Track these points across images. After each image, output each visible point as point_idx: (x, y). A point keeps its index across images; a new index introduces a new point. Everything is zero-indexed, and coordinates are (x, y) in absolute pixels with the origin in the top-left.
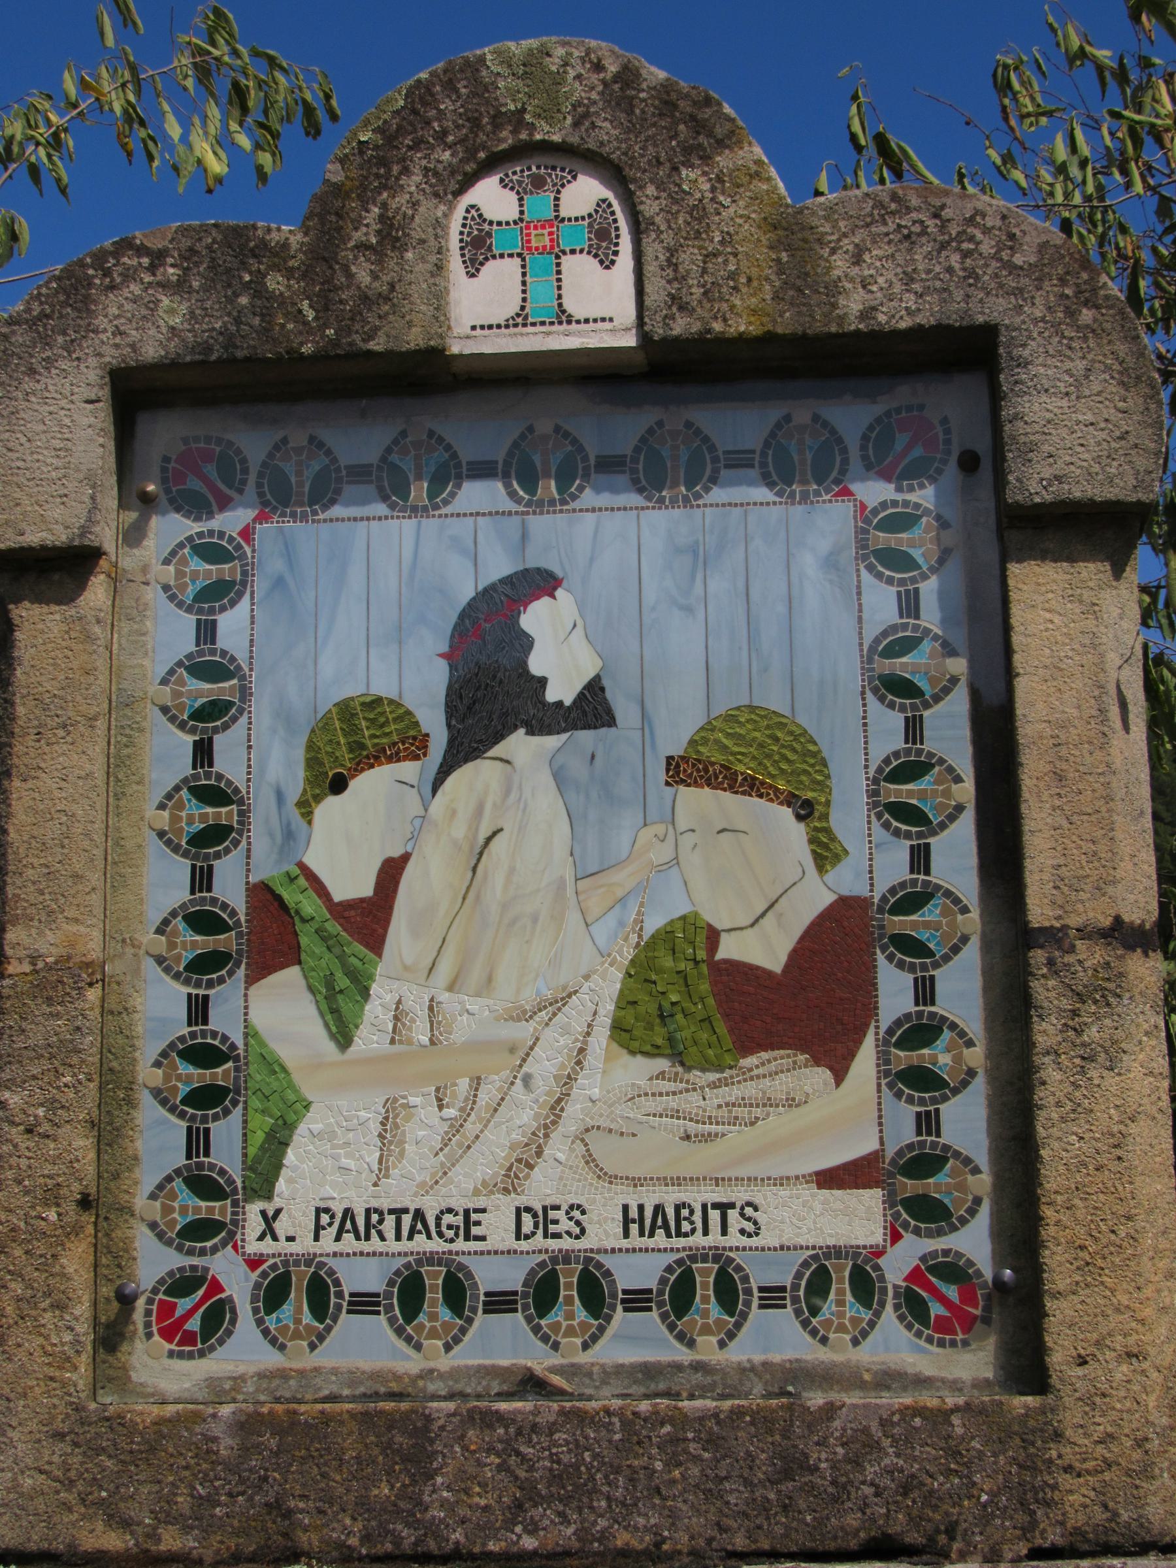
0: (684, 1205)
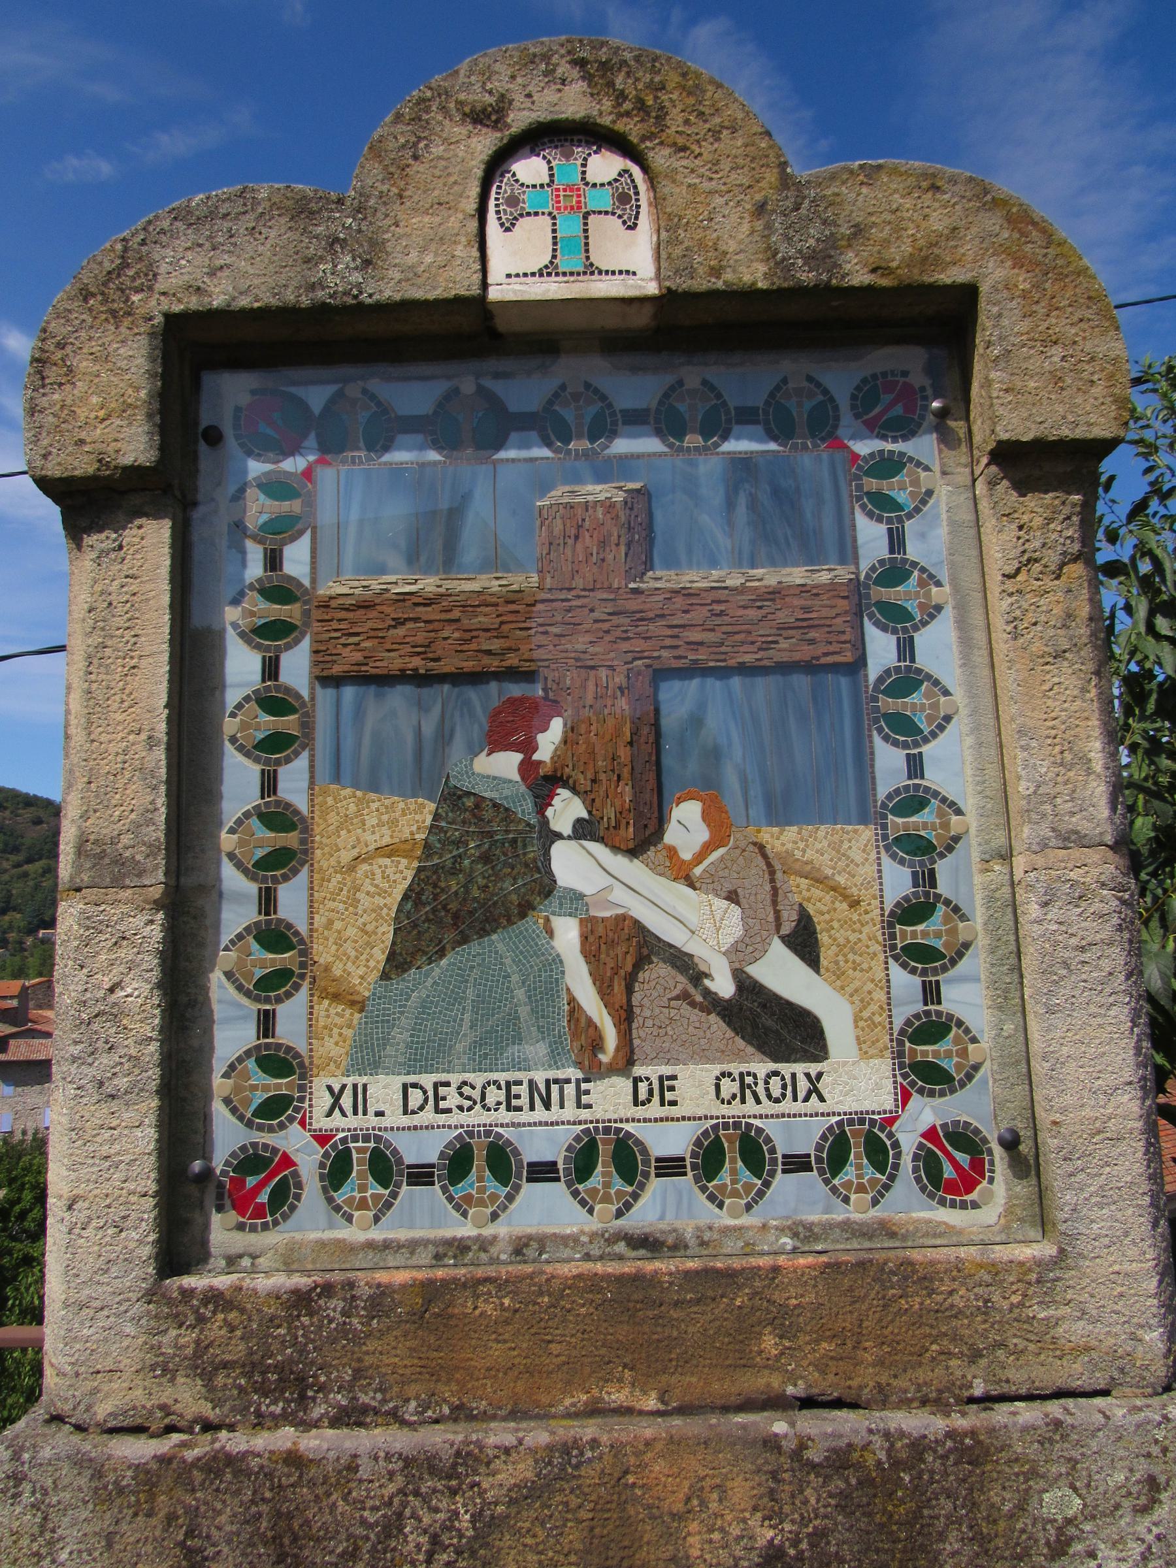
0: (749, 1074)
